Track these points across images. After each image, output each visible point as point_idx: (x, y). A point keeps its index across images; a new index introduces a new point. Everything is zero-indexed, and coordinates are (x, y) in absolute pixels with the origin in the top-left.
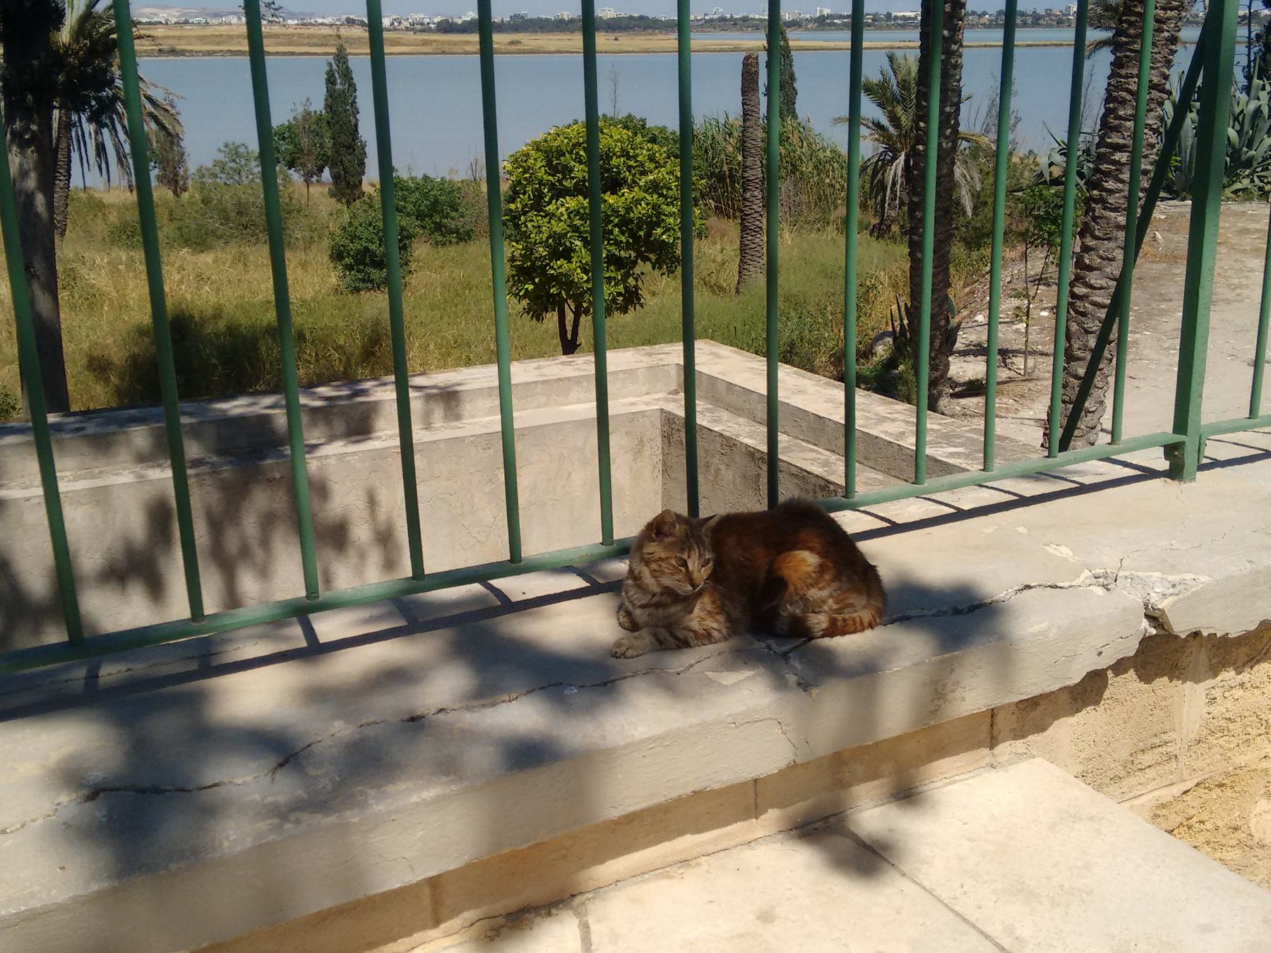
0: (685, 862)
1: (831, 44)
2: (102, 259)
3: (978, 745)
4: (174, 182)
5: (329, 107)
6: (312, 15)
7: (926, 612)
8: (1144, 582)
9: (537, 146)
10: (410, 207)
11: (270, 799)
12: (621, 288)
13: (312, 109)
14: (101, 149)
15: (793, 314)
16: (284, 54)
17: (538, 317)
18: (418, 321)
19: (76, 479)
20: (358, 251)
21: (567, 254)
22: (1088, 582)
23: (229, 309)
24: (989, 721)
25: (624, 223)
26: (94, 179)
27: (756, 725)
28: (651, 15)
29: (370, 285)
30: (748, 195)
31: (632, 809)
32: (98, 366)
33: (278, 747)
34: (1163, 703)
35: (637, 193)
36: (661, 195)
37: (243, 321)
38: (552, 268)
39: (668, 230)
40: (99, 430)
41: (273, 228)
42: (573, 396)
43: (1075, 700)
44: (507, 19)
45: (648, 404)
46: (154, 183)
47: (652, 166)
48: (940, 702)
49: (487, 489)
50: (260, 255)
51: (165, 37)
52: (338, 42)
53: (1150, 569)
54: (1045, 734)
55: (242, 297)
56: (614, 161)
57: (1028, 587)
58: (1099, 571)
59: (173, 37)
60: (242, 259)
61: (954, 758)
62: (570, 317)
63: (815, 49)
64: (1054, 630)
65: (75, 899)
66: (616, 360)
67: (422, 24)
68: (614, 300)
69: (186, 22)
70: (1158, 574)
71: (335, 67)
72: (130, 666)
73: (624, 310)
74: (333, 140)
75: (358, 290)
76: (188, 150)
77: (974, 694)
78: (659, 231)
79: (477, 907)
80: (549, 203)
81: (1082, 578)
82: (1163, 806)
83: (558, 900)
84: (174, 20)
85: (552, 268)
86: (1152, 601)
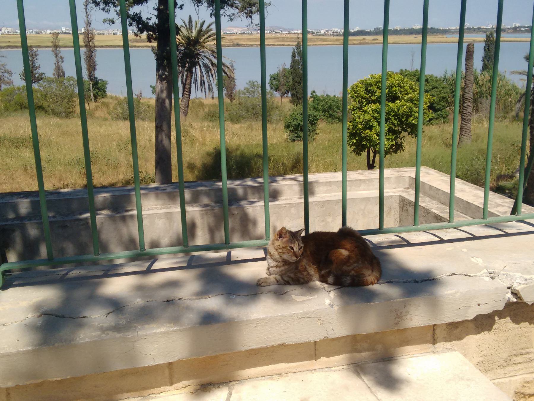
0: (281, 374)
1: (519, 39)
2: (198, 126)
3: (426, 342)
4: (231, 96)
5: (292, 66)
6: (293, 30)
7: (400, 280)
8: (512, 278)
9: (362, 82)
10: (320, 107)
11: (101, 325)
12: (394, 143)
13: (286, 67)
14: (202, 82)
15: (481, 158)
16: (280, 45)
17: (358, 154)
18: (316, 154)
19: (161, 209)
20: (296, 125)
21: (371, 128)
22: (485, 275)
23: (242, 147)
24: (431, 332)
25: (396, 115)
26: (200, 95)
27: (308, 319)
28: (436, 27)
29: (299, 139)
30: (465, 105)
31: (251, 348)
32: (191, 167)
33: (116, 305)
34: (526, 335)
35: (403, 102)
36: (413, 104)
37: (247, 151)
38: (364, 133)
39: (415, 118)
40: (171, 190)
41: (264, 113)
42: (362, 187)
43: (478, 328)
44: (373, 30)
45: (394, 192)
46: (224, 96)
47: (411, 91)
48: (399, 320)
49: (321, 224)
50: (258, 125)
51: (235, 39)
52: (297, 40)
53: (517, 272)
54: (461, 341)
55: (249, 142)
56: (394, 89)
57: (454, 274)
58: (491, 271)
59: (238, 39)
60: (250, 127)
61: (414, 346)
62: (372, 155)
63: (511, 41)
64: (459, 294)
65: (19, 353)
66: (387, 172)
67: (337, 32)
68: (391, 147)
69: (244, 33)
70: (520, 274)
71: (296, 50)
72: (80, 271)
73: (396, 152)
74: (295, 80)
75: (294, 141)
76: (236, 84)
77: (418, 316)
78: (411, 119)
79: (189, 380)
80: (365, 106)
81: (482, 272)
82: (528, 382)
83: (226, 381)
84: (239, 32)
85: (364, 133)
86: (514, 286)
